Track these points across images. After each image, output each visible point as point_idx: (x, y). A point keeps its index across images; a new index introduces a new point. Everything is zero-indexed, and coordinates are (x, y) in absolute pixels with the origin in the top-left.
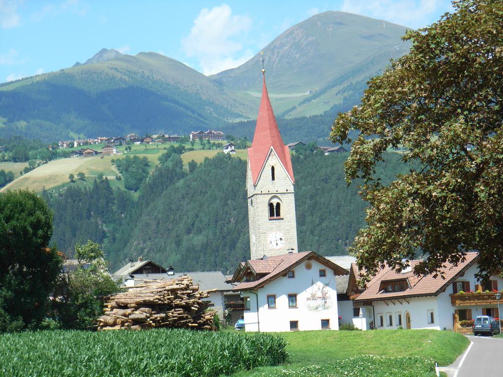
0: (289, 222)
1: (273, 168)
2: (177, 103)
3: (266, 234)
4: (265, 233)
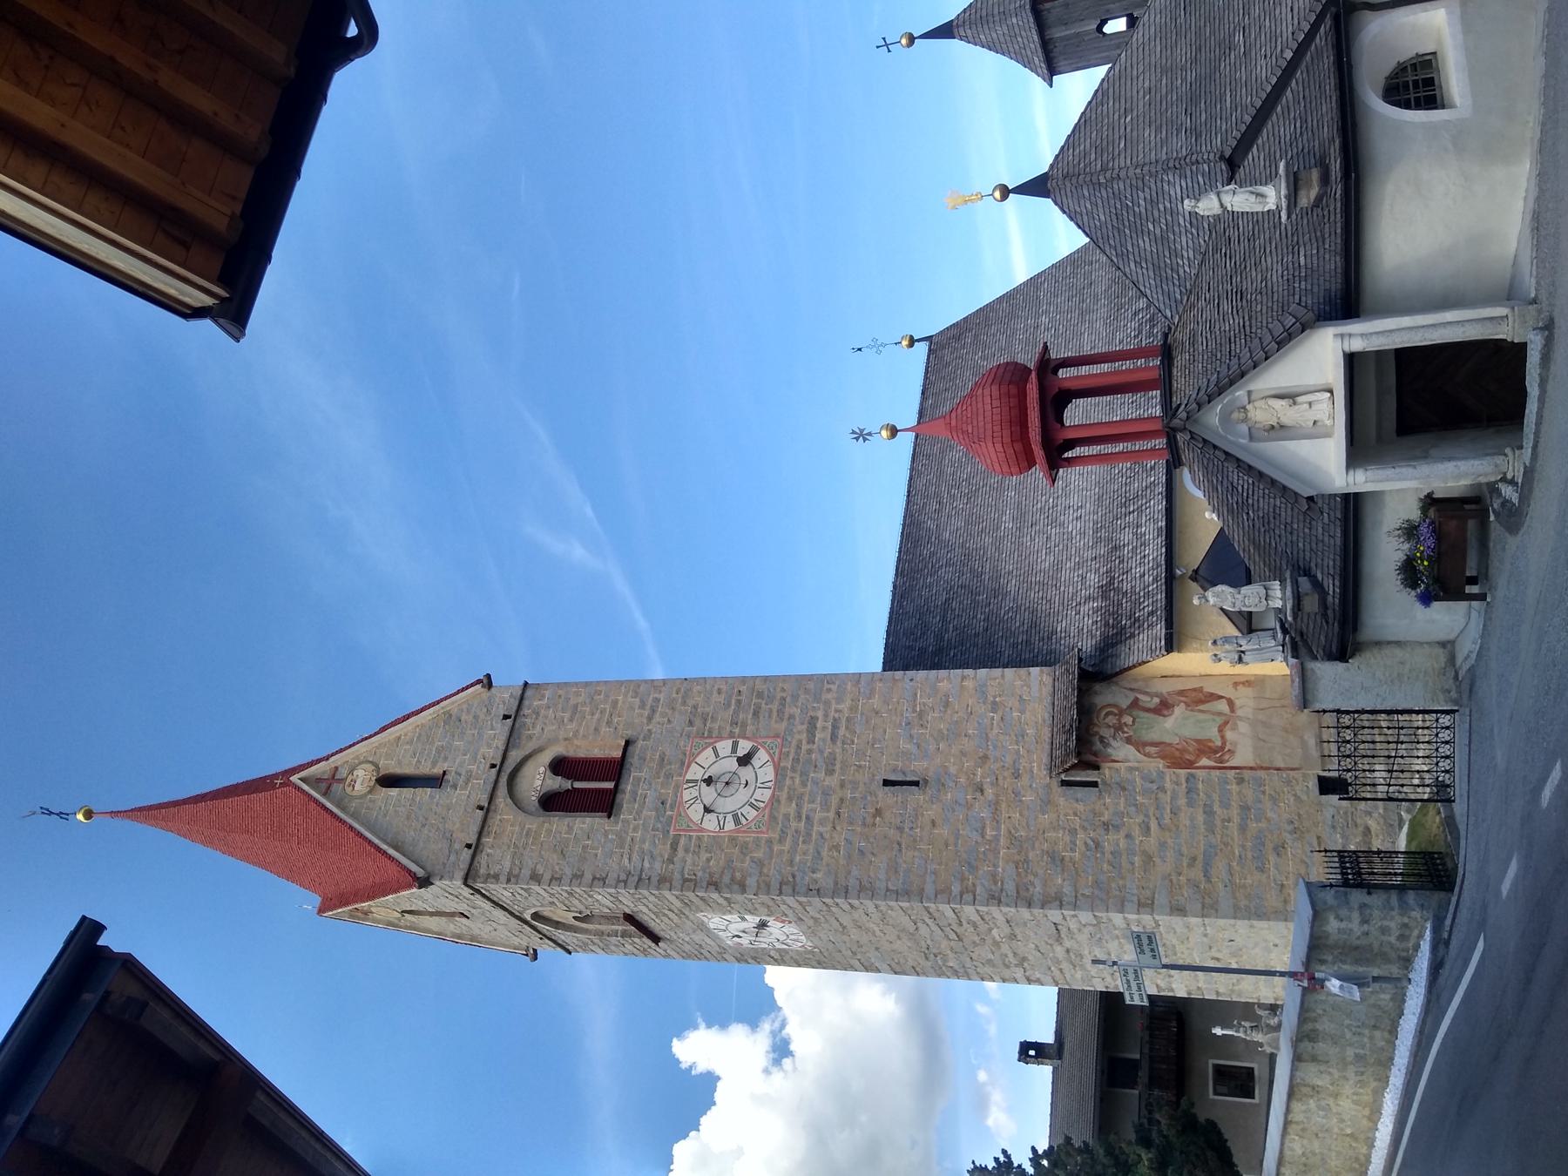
0: (653, 711)
1: (390, 781)
2: (1385, 345)
3: (682, 841)
4: (674, 847)
